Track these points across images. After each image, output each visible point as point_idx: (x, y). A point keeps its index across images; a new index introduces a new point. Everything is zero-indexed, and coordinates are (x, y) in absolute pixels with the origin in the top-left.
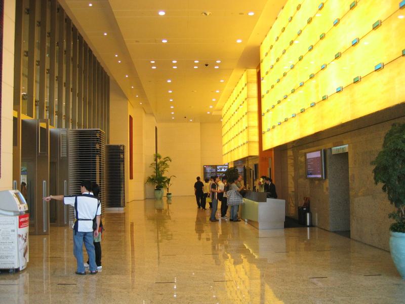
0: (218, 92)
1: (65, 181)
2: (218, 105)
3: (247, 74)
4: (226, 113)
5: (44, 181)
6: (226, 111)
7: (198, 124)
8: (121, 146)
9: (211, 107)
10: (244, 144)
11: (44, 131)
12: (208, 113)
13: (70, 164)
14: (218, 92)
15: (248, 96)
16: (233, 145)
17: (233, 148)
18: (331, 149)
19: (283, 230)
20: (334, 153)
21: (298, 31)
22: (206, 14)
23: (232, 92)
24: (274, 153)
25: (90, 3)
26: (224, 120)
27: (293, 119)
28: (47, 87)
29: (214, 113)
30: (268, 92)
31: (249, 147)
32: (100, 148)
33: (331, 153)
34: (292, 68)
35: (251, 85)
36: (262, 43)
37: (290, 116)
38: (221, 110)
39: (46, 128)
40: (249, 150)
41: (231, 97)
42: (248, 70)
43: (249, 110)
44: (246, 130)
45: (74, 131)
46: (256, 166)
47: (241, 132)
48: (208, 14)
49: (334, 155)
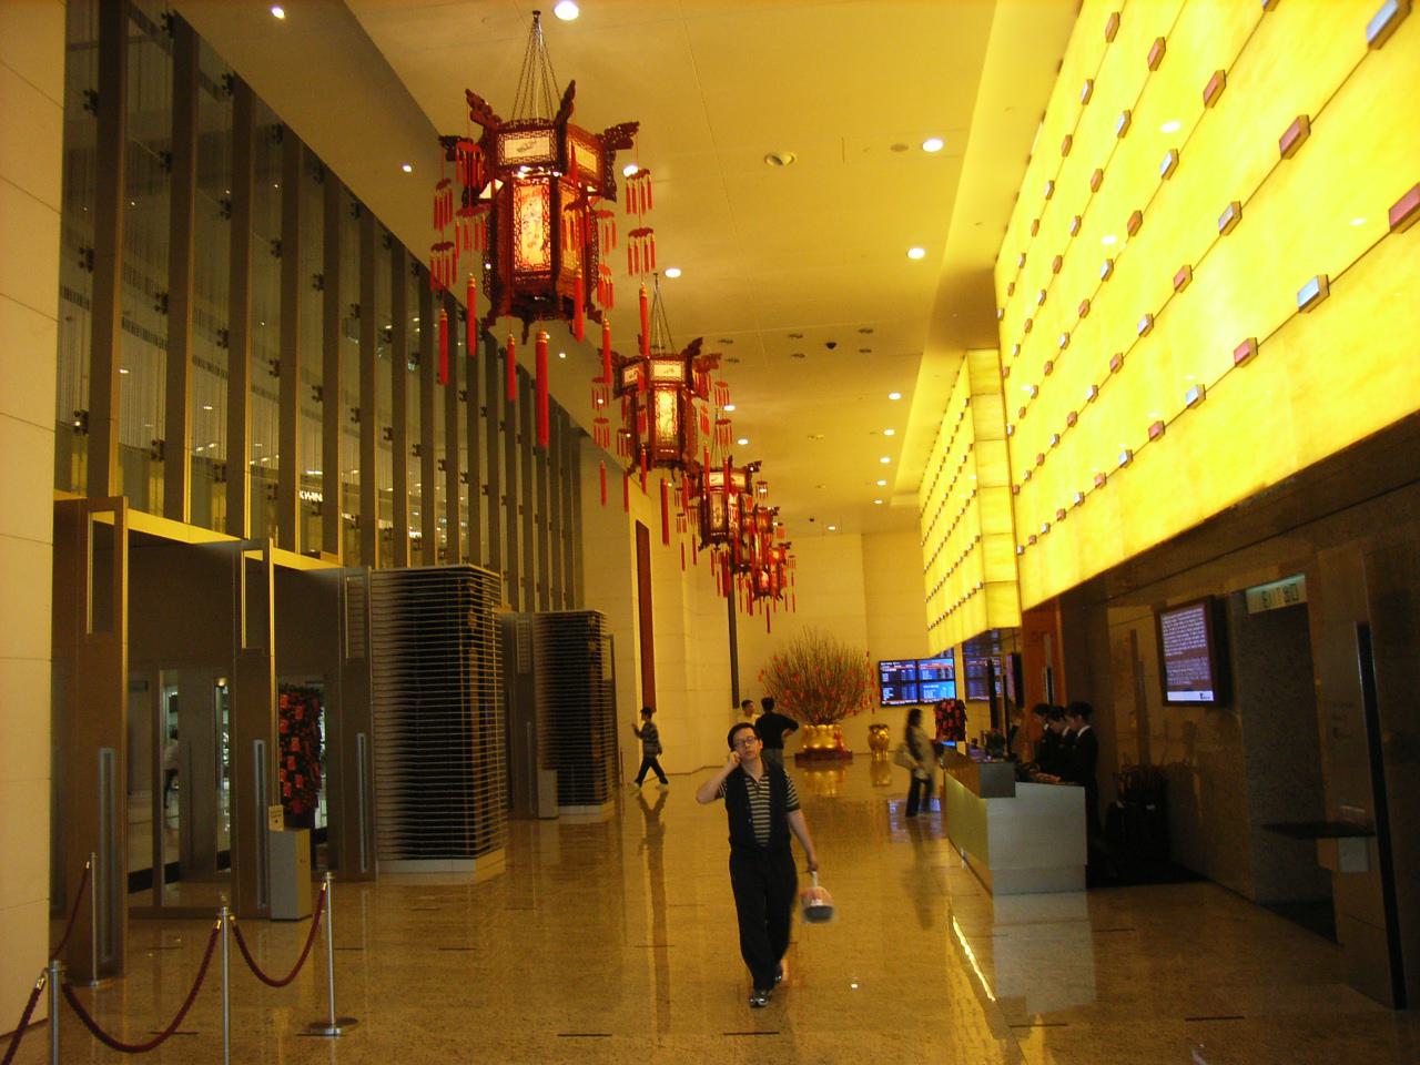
0: (889, 432)
1: (529, 724)
2: (903, 476)
3: (969, 366)
4: (929, 498)
5: (360, 735)
6: (928, 493)
7: (854, 541)
8: (591, 613)
9: (882, 483)
10: (975, 591)
11: (258, 569)
12: (878, 502)
13: (537, 682)
14: (889, 432)
15: (975, 436)
16: (948, 598)
17: (948, 608)
18: (1243, 593)
19: (1083, 896)
20: (1255, 607)
21: (1090, 174)
22: (778, 161)
23: (938, 433)
24: (1062, 614)
25: (407, 164)
26: (926, 522)
27: (1100, 494)
28: (718, 518)
29: (895, 502)
30: (1023, 413)
31: (988, 601)
32: (480, 625)
33: (1246, 608)
34: (1085, 310)
35: (983, 402)
36: (997, 258)
37: (1089, 486)
38: (917, 491)
39: (261, 559)
40: (988, 613)
41: (937, 447)
42: (971, 354)
43: (981, 481)
44: (977, 546)
45: (394, 575)
46: (1016, 659)
47: (966, 553)
48: (786, 159)
49: (1255, 616)
